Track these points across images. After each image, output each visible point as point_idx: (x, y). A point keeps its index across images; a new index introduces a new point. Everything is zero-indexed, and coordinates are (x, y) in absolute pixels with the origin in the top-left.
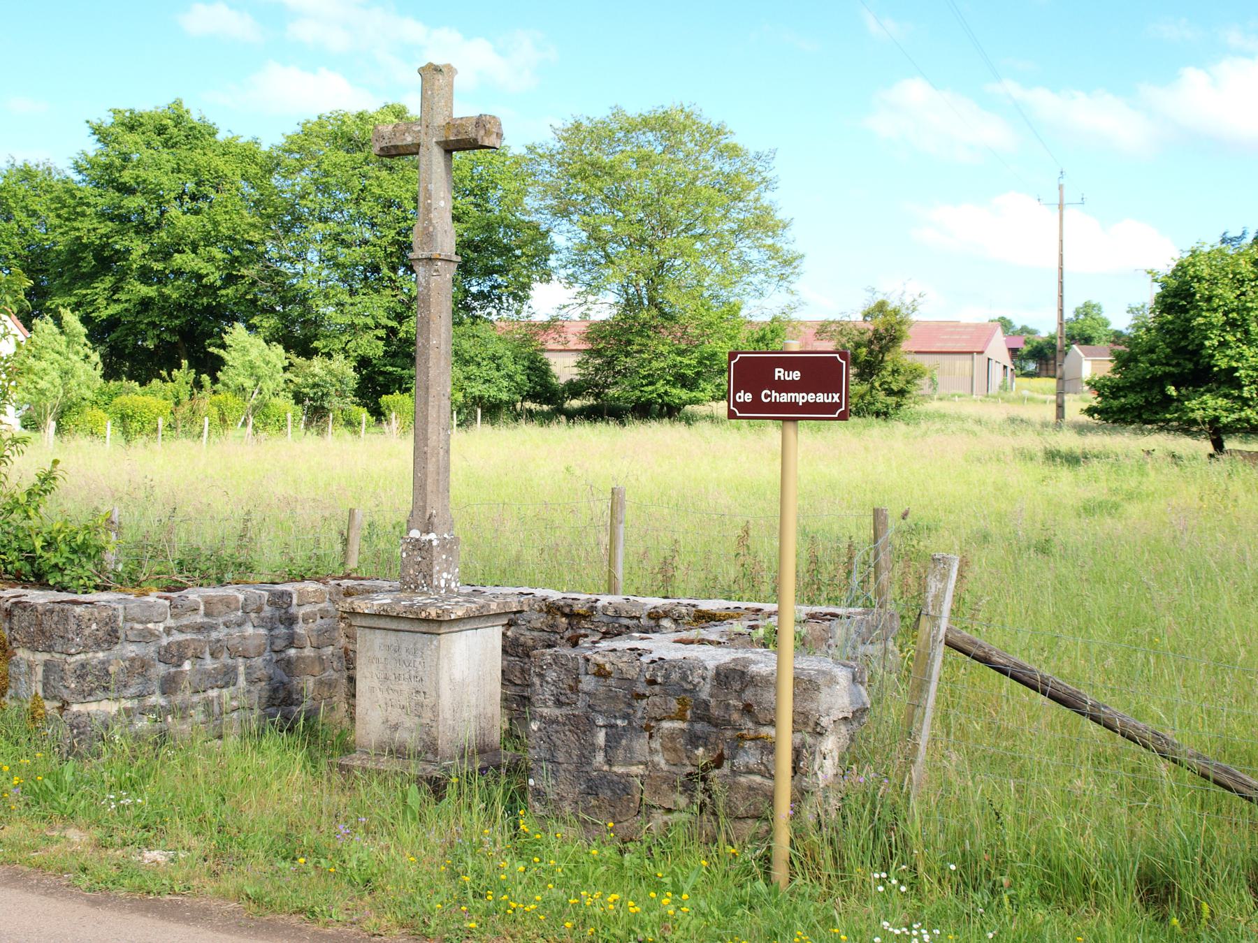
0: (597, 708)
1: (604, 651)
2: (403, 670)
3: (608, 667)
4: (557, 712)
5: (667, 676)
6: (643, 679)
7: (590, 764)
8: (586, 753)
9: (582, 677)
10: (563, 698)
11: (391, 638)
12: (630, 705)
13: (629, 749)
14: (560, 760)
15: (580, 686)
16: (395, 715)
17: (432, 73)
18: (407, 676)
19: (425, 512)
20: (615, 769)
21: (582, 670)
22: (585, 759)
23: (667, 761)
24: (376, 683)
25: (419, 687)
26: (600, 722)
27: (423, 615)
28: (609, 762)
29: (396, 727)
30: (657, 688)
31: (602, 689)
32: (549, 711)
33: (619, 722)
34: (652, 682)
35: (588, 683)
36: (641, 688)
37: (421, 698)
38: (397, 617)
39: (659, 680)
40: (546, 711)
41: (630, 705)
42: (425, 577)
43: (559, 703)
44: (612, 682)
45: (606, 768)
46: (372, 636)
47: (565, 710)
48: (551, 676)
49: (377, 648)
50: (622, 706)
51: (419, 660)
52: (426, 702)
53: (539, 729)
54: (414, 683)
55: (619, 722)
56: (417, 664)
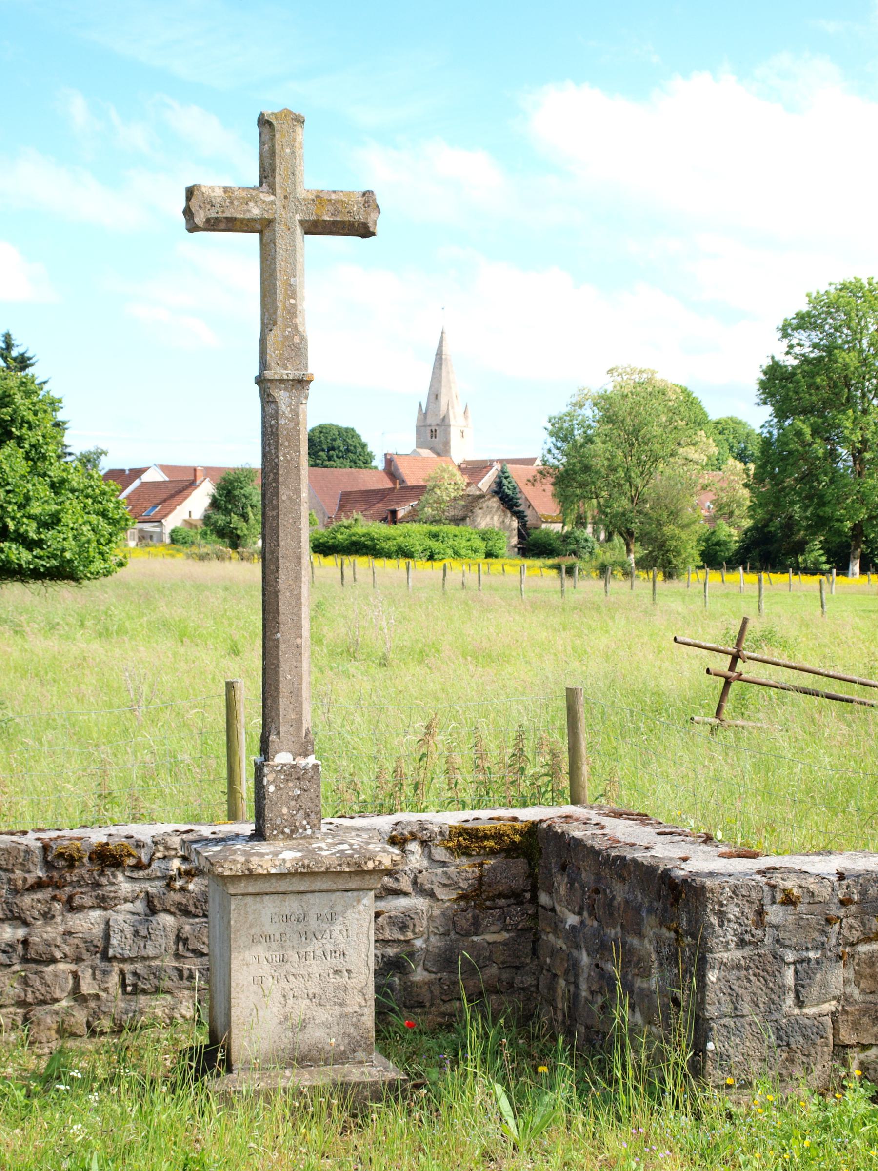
0: (787, 942)
3: (795, 891)
4: (739, 954)
5: (863, 893)
6: (836, 901)
7: (778, 1010)
8: (776, 998)
9: (767, 908)
10: (747, 937)
11: (292, 905)
12: (824, 933)
13: (824, 985)
14: (745, 1012)
15: (767, 919)
16: (301, 1008)
17: (272, 133)
18: (319, 953)
19: (299, 727)
20: (806, 1011)
21: (767, 900)
22: (773, 1006)
23: (863, 991)
24: (266, 969)
25: (338, 963)
26: (790, 957)
27: (371, 865)
28: (800, 1003)
29: (303, 1025)
30: (853, 908)
31: (791, 918)
32: (735, 955)
33: (812, 955)
34: (843, 903)
35: (775, 914)
36: (835, 911)
39: (856, 897)
40: (725, 956)
41: (824, 933)
42: (308, 815)
43: (742, 943)
44: (802, 908)
45: (796, 1011)
47: (747, 951)
48: (733, 911)
49: (266, 919)
50: (816, 935)
52: (351, 983)
53: (719, 979)
55: (812, 955)
56: (334, 935)
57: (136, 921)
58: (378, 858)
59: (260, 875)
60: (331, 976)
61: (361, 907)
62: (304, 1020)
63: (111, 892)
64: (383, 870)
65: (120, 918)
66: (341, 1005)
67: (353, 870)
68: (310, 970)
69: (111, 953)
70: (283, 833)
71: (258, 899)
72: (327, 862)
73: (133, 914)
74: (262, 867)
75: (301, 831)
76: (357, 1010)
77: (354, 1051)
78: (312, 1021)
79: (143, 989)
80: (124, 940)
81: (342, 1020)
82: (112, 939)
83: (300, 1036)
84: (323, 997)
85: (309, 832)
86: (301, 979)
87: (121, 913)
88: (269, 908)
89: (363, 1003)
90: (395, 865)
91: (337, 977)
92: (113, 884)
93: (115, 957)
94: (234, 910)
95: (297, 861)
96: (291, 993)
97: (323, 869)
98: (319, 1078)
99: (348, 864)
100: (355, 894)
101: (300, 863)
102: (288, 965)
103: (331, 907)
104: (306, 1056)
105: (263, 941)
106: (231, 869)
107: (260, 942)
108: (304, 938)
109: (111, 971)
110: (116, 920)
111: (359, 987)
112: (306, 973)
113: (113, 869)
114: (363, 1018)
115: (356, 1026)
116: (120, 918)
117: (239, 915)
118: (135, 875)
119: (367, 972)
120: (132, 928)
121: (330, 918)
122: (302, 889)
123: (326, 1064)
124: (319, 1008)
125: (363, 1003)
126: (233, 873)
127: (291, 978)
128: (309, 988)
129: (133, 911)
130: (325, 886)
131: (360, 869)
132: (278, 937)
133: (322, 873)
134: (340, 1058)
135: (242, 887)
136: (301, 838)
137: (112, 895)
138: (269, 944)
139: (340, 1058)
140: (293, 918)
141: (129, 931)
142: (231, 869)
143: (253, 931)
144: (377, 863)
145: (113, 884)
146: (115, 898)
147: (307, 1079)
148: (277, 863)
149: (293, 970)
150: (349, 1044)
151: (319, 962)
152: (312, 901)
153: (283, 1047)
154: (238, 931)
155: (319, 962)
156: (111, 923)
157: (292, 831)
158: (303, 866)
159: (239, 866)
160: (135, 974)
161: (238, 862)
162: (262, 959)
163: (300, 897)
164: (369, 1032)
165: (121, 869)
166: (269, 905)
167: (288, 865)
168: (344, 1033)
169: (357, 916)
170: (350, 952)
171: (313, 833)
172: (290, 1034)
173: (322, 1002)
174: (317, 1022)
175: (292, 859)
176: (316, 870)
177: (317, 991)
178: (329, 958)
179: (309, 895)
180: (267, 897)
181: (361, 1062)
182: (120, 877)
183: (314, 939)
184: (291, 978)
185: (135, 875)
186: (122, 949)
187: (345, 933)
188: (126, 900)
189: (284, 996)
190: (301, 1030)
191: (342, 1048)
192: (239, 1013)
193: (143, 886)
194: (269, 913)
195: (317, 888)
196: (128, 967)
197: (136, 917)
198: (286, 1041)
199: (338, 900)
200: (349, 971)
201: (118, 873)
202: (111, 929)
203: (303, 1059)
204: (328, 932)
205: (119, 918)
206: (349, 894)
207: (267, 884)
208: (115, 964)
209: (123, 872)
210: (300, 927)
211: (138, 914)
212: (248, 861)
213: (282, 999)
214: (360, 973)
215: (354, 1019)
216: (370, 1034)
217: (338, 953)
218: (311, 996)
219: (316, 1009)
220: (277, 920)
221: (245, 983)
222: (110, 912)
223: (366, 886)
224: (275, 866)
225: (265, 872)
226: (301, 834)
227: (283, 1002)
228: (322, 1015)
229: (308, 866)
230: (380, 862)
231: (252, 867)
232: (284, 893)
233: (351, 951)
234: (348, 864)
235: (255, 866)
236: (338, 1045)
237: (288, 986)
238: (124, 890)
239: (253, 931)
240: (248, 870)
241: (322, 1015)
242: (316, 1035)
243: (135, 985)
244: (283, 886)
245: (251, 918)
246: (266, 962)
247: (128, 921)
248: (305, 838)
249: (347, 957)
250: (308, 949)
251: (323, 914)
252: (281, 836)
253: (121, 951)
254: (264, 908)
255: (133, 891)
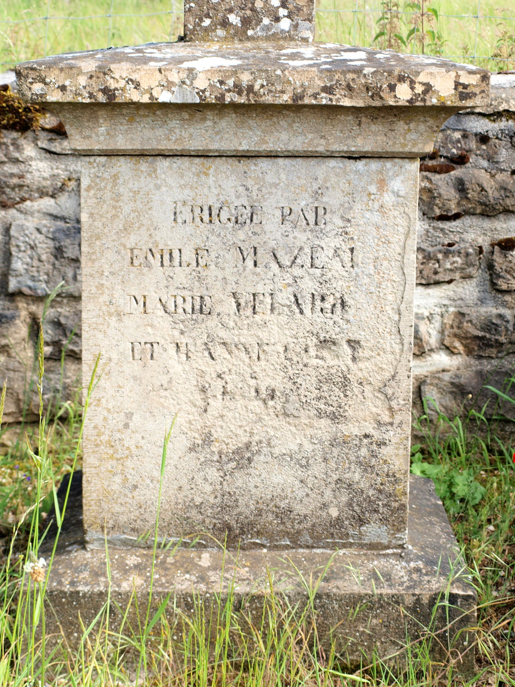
1: (349, 63)
2: (268, 280)
11: (223, 184)
16: (235, 422)
18: (285, 297)
25: (331, 325)
27: (403, 94)
29: (243, 458)
37: (340, 360)
38: (296, 108)
46: (144, 183)
49: (162, 215)
51: (331, 243)
52: (358, 371)
54: (313, 319)
56: (322, 258)
57: (59, 230)
58: (422, 78)
59: (138, 106)
60: (313, 352)
61: (388, 199)
62: (248, 446)
63: (12, 175)
64: (433, 108)
65: (30, 223)
66: (334, 417)
67: (360, 103)
68: (263, 335)
69: (13, 285)
70: (225, 24)
71: (144, 165)
72: (297, 80)
73: (56, 217)
74: (137, 86)
75: (266, 21)
76: (370, 431)
77: (361, 521)
78: (265, 450)
79: (72, 351)
80: (36, 263)
81: (336, 451)
82: (14, 260)
83: (240, 480)
84: (293, 398)
85: (285, 24)
86: (243, 355)
87: (32, 214)
88: (170, 186)
89: (386, 418)
90: (463, 96)
91: (325, 353)
92: (16, 161)
93: (20, 293)
94: (89, 188)
95: (223, 75)
96: (220, 383)
97: (286, 98)
98: (275, 578)
99: (349, 88)
100: (374, 165)
101: (230, 82)
102: (212, 322)
103: (317, 194)
104: (251, 524)
105: (156, 262)
106: (63, 88)
107: (149, 266)
108: (250, 263)
109: (13, 317)
110: (22, 228)
111: (377, 380)
112: (253, 341)
113: (15, 135)
114: (384, 450)
115: (366, 467)
116: (30, 223)
117: (100, 200)
118: (57, 147)
119: (397, 348)
120: (51, 244)
121: (312, 221)
122: (244, 146)
123: (296, 544)
124: (282, 422)
125: (386, 418)
126: (69, 98)
127: (219, 351)
128: (260, 375)
129: (55, 212)
130: (298, 144)
131: (377, 103)
132: (189, 255)
133: (285, 107)
134: (330, 534)
135: (101, 134)
136: (267, 38)
137: (15, 181)
138: (169, 271)
139: (330, 534)
140: (224, 216)
141: (44, 249)
142: (63, 88)
143: (131, 240)
144: (419, 89)
145: (16, 161)
146: (21, 186)
147: (232, 576)
148: (175, 77)
149: (223, 333)
150: (350, 505)
151: (283, 319)
152: (270, 178)
153: (198, 500)
154: (98, 238)
155: (283, 319)
156: (13, 232)
157: (246, 22)
158: (238, 88)
159: (83, 81)
160: (57, 324)
161: (80, 72)
162: (153, 304)
163: (243, 165)
164: (397, 481)
165: (29, 134)
166: (170, 181)
167: (201, 83)
168: (339, 481)
169: (376, 218)
170: (356, 299)
171: (296, 27)
172: (213, 474)
173: (290, 408)
174: (276, 451)
175: (212, 71)
176: (269, 99)
177: (279, 383)
178: (307, 310)
179: (264, 164)
180: (166, 163)
181: (375, 546)
182: (29, 150)
183: (274, 266)
184: (219, 351)
185: (57, 147)
186: (33, 278)
187: (347, 257)
188: (43, 193)
189: (203, 390)
190: (239, 467)
191: (334, 513)
192: (98, 421)
193: (72, 167)
194: (169, 200)
195: (279, 147)
196: (45, 312)
197: (60, 224)
198: (208, 489)
199: (334, 179)
200: (354, 344)
201: (22, 142)
202: (13, 242)
203: (236, 532)
204: (307, 250)
205: (27, 224)
206: (360, 165)
207: (160, 132)
208: (22, 304)
209: (35, 140)
210: (241, 235)
211: (63, 219)
212: (104, 71)
213: (198, 397)
214: (380, 350)
215: (364, 452)
216: (399, 487)
217: (331, 300)
218: (264, 394)
219: (276, 423)
220: (188, 216)
221: (115, 356)
222: (12, 212)
223: (398, 149)
224: (168, 86)
225: (145, 99)
226: (268, 28)
227: (201, 403)
228: (290, 438)
229: (250, 89)
230: (428, 88)
231: (112, 84)
232: (204, 155)
233: (361, 298)
234: (349, 88)
235: (122, 84)
236: (325, 506)
237: (211, 369)
238: (37, 174)
239: (131, 240)
240: (105, 91)
241: (290, 438)
242: (272, 481)
243: (56, 344)
244: (198, 136)
245: (126, 209)
246: (161, 313)
247: (44, 230)
248: (274, 37)
249: (351, 311)
250: (260, 289)
251: (296, 209)
252: (220, 32)
253: (30, 283)
254: (158, 187)
255: (54, 176)
